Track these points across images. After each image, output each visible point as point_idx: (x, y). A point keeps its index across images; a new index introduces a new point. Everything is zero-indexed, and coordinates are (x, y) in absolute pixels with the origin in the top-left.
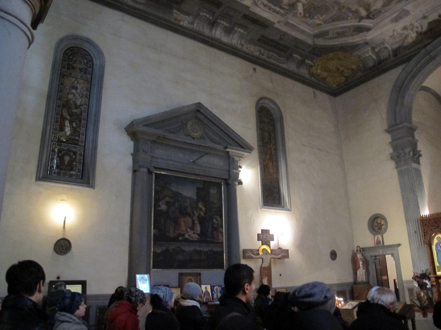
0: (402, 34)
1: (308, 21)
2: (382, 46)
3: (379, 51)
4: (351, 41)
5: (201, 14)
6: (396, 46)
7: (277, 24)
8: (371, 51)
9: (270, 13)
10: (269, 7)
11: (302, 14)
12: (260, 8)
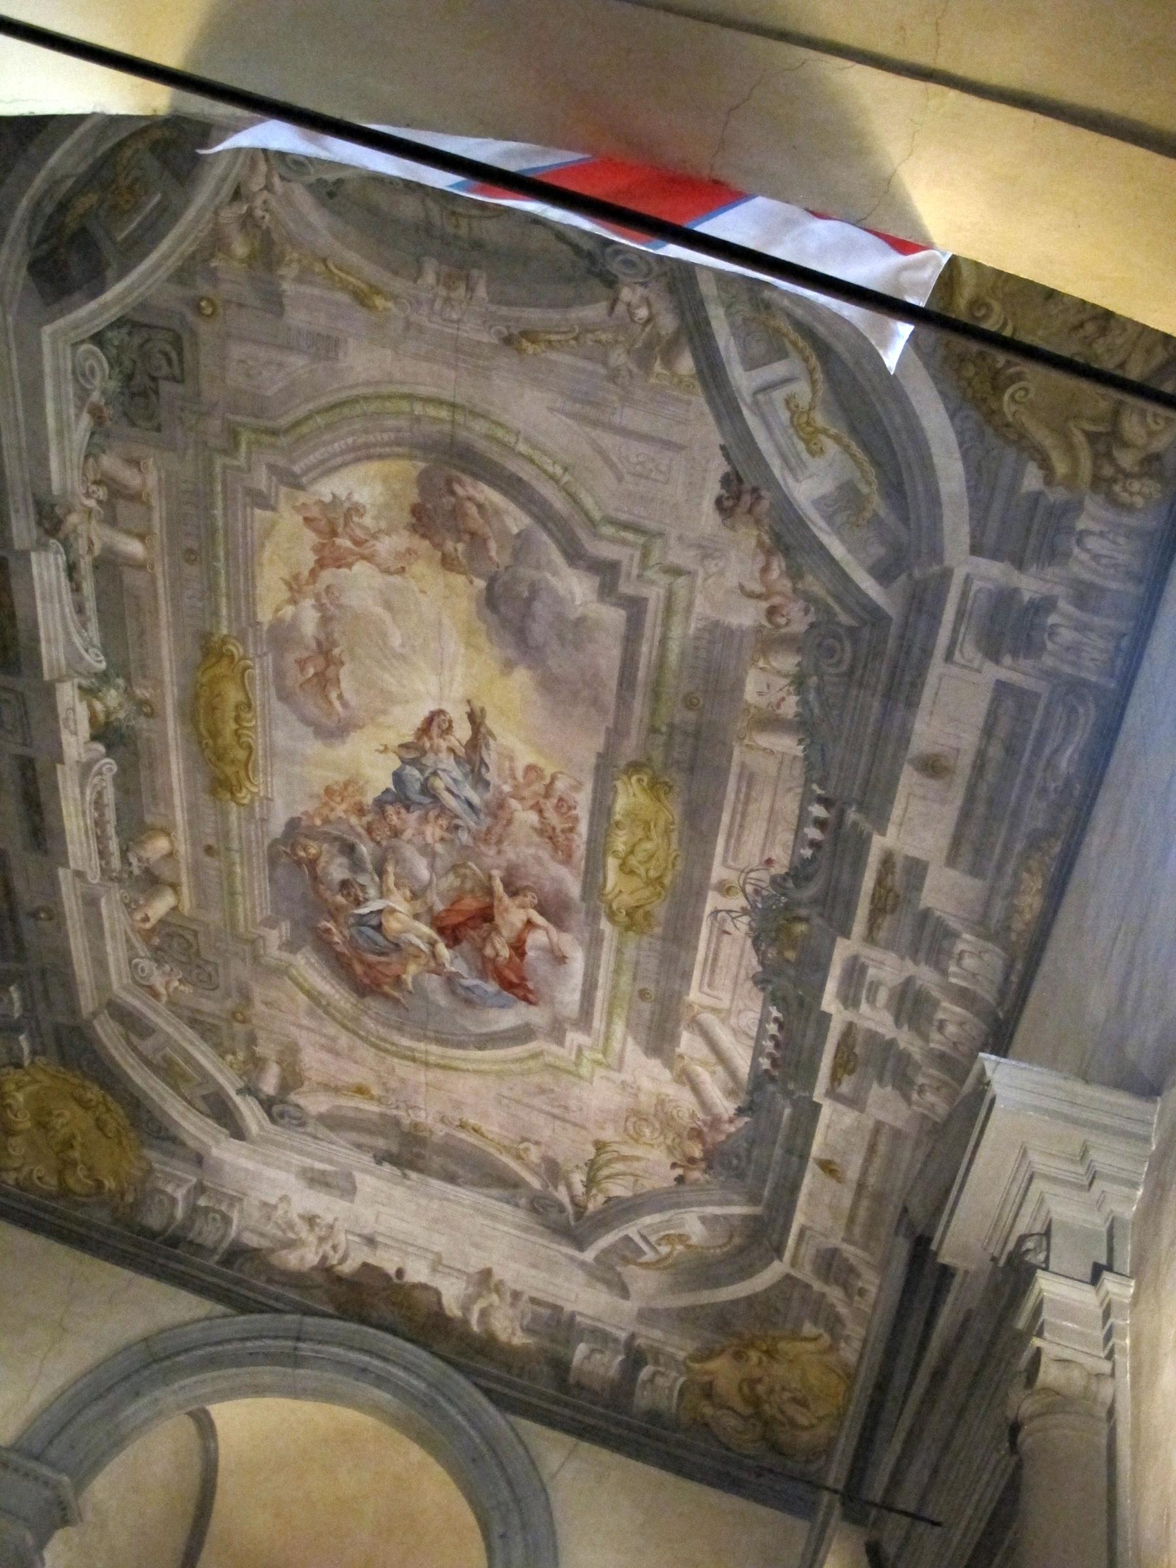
0: (291, 1226)
2: (223, 1208)
6: (252, 1240)
8: (189, 1191)
11: (148, 926)
12: (83, 793)
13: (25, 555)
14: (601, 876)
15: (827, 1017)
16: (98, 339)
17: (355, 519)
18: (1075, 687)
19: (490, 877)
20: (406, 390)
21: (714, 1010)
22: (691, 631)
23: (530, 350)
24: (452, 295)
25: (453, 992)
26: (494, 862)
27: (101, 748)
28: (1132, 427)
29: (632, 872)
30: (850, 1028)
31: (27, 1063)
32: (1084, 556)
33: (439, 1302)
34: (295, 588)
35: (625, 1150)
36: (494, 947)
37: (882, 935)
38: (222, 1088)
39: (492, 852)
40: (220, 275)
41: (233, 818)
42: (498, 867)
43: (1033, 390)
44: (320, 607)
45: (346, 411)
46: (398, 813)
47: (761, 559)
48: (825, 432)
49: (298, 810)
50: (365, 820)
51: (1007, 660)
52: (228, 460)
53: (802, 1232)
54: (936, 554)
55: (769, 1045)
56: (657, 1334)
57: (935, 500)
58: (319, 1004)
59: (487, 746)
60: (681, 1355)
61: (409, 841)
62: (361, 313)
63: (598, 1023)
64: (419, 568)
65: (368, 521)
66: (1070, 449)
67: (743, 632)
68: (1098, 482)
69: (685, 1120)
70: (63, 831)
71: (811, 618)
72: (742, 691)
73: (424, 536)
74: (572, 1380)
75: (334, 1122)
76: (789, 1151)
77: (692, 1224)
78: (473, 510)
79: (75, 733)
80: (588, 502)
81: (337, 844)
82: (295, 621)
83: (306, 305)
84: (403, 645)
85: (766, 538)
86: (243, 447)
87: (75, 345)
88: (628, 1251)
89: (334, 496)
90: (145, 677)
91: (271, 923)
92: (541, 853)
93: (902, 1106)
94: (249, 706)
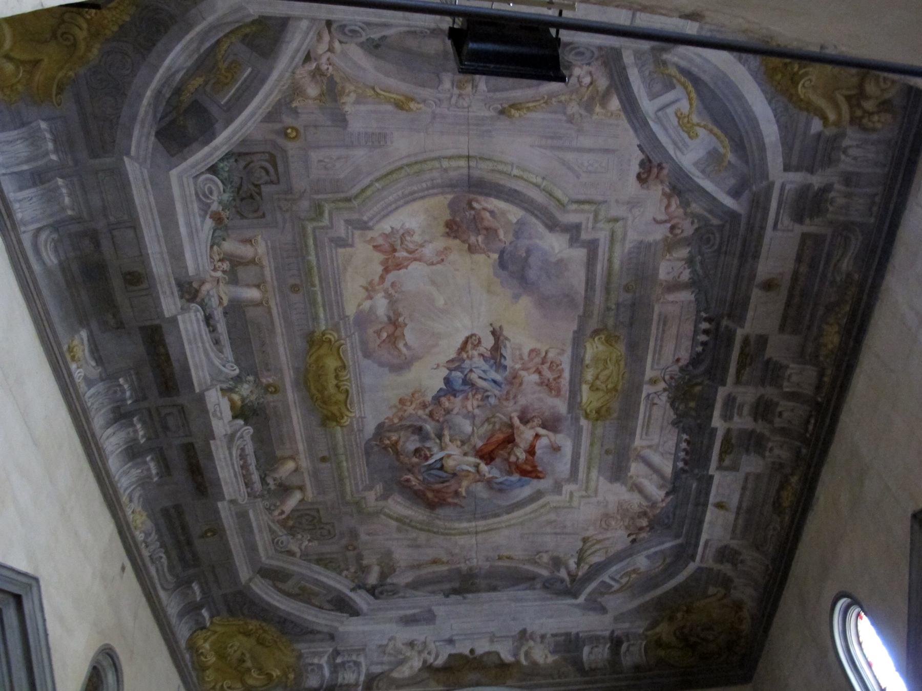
1: (280, 534)
3: (343, 663)
4: (310, 618)
5: (121, 381)
7: (225, 503)
8: (329, 657)
9: (236, 476)
10: (245, 462)
11: (284, 516)
12: (231, 454)
13: (174, 320)
14: (579, 397)
15: (714, 431)
16: (213, 170)
17: (408, 238)
18: (848, 226)
19: (511, 418)
20: (437, 154)
21: (650, 447)
22: (626, 251)
23: (517, 115)
24: (463, 92)
25: (491, 488)
26: (512, 410)
27: (241, 422)
28: (871, 88)
29: (597, 389)
30: (729, 431)
31: (208, 624)
32: (848, 160)
34: (370, 290)
35: (600, 537)
36: (516, 455)
37: (744, 378)
38: (340, 592)
39: (511, 403)
40: (299, 111)
41: (339, 436)
42: (516, 411)
43: (814, 79)
44: (388, 296)
45: (395, 176)
46: (449, 400)
47: (665, 201)
48: (698, 125)
49: (382, 419)
50: (427, 411)
51: (807, 221)
52: (315, 224)
53: (707, 542)
54: (765, 175)
55: (682, 454)
56: (627, 625)
57: (762, 148)
58: (404, 523)
59: (505, 347)
60: (641, 631)
61: (457, 414)
62: (403, 115)
63: (582, 475)
64: (453, 257)
65: (416, 238)
66: (836, 106)
67: (656, 243)
68: (853, 120)
69: (636, 508)
70: (218, 479)
71: (696, 226)
72: (658, 274)
73: (455, 237)
74: (587, 669)
75: (415, 585)
76: (697, 505)
77: (641, 562)
78: (487, 215)
79: (221, 418)
80: (559, 194)
81: (410, 430)
82: (372, 309)
83: (360, 116)
84: (446, 304)
85: (667, 190)
86: (326, 215)
87: (197, 177)
88: (605, 589)
89: (392, 228)
90: (269, 370)
91: (370, 488)
92: (541, 395)
93: (761, 462)
94: (344, 367)
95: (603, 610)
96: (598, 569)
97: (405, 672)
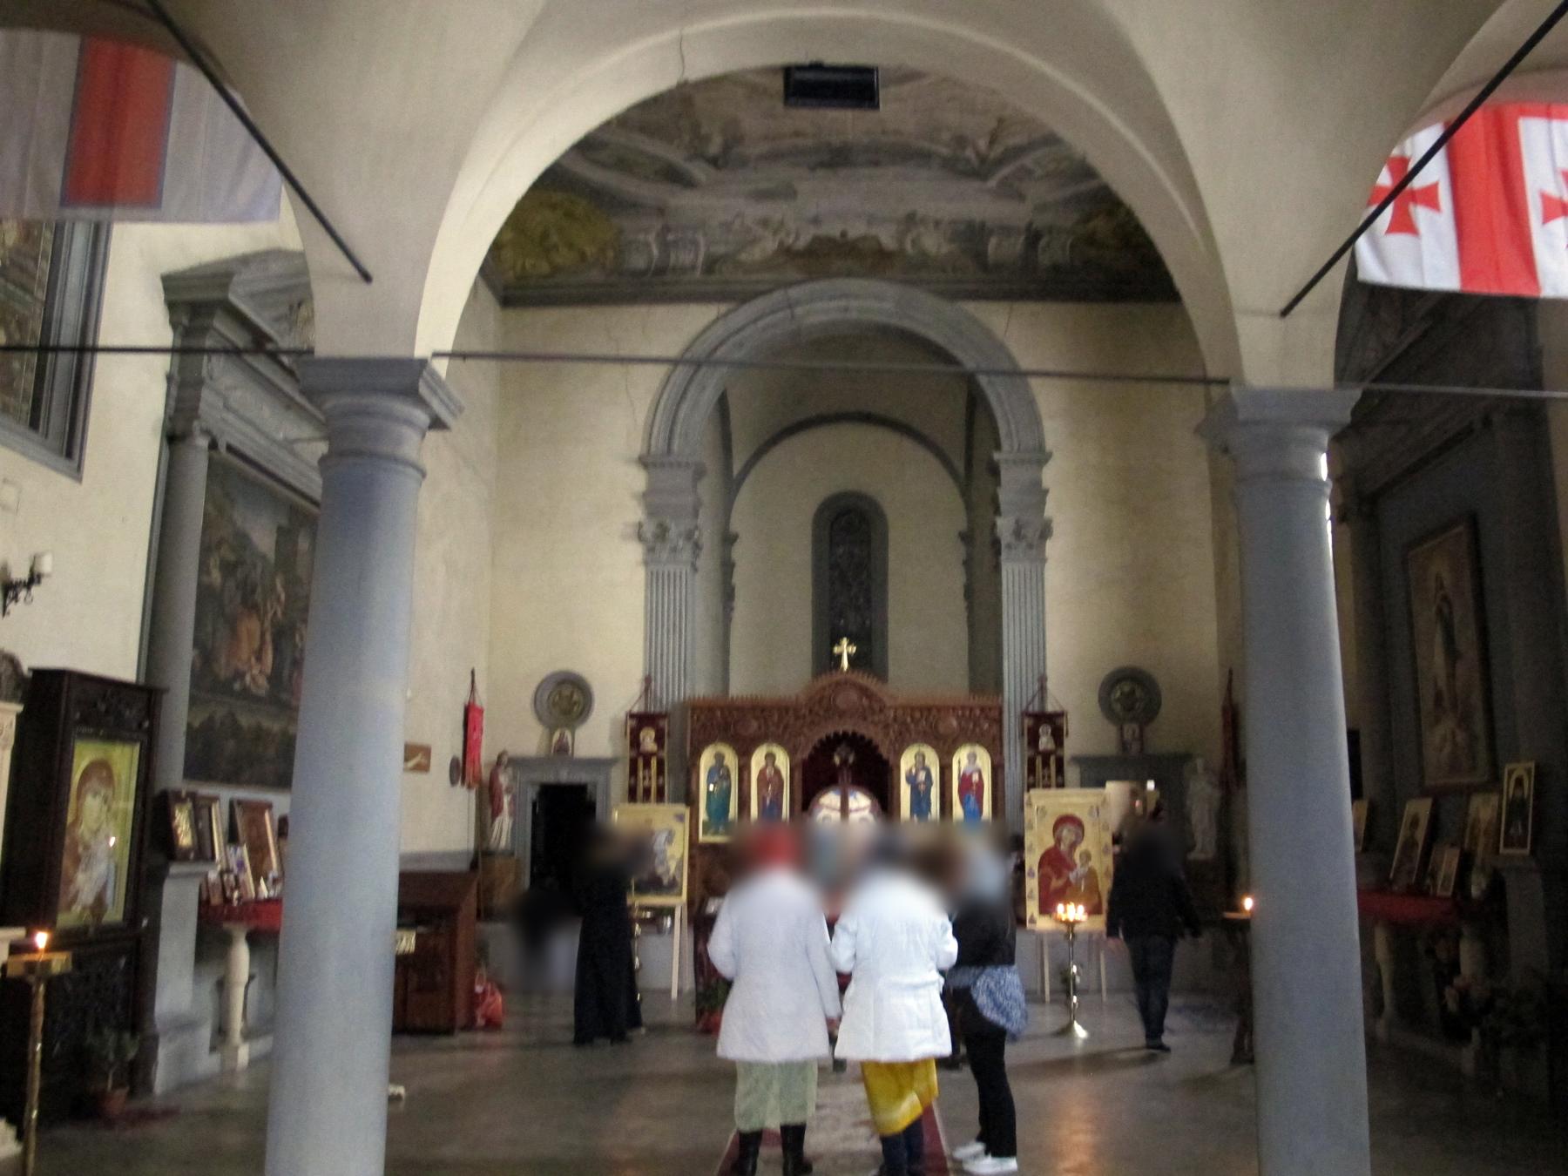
3: (675, 242)
33: (880, 244)
75: (774, 157)
88: (1027, 173)
95: (1021, 197)
96: (1019, 151)
97: (756, 254)
